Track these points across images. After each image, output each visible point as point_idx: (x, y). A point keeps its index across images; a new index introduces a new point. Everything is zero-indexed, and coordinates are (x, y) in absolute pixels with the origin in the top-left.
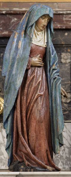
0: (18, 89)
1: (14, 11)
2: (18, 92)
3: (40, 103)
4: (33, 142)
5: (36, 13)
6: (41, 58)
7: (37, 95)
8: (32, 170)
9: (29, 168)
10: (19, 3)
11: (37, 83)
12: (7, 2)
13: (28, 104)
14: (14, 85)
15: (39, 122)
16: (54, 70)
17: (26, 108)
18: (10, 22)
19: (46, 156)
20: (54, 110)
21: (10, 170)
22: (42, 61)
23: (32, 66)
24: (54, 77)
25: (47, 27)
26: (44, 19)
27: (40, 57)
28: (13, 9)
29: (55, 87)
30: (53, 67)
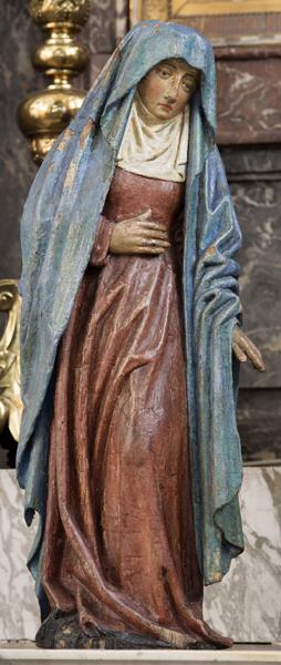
1: (242, 47)
4: (115, 539)
5: (133, 54)
7: (126, 360)
8: (102, 643)
9: (88, 636)
10: (266, 14)
11: (132, 316)
12: (225, 16)
13: (95, 396)
15: (134, 462)
16: (208, 265)
17: (88, 413)
19: (161, 589)
20: (204, 417)
21: (43, 640)
22: (164, 235)
23: (113, 254)
24: (207, 294)
26: (171, 75)
28: (239, 40)
29: (210, 332)
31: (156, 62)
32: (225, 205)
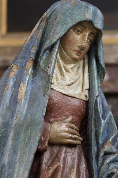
16: (107, 154)
23: (51, 144)
24: (109, 172)
25: (89, 53)
26: (82, 32)
27: (71, 122)
31: (74, 23)
32: (110, 118)
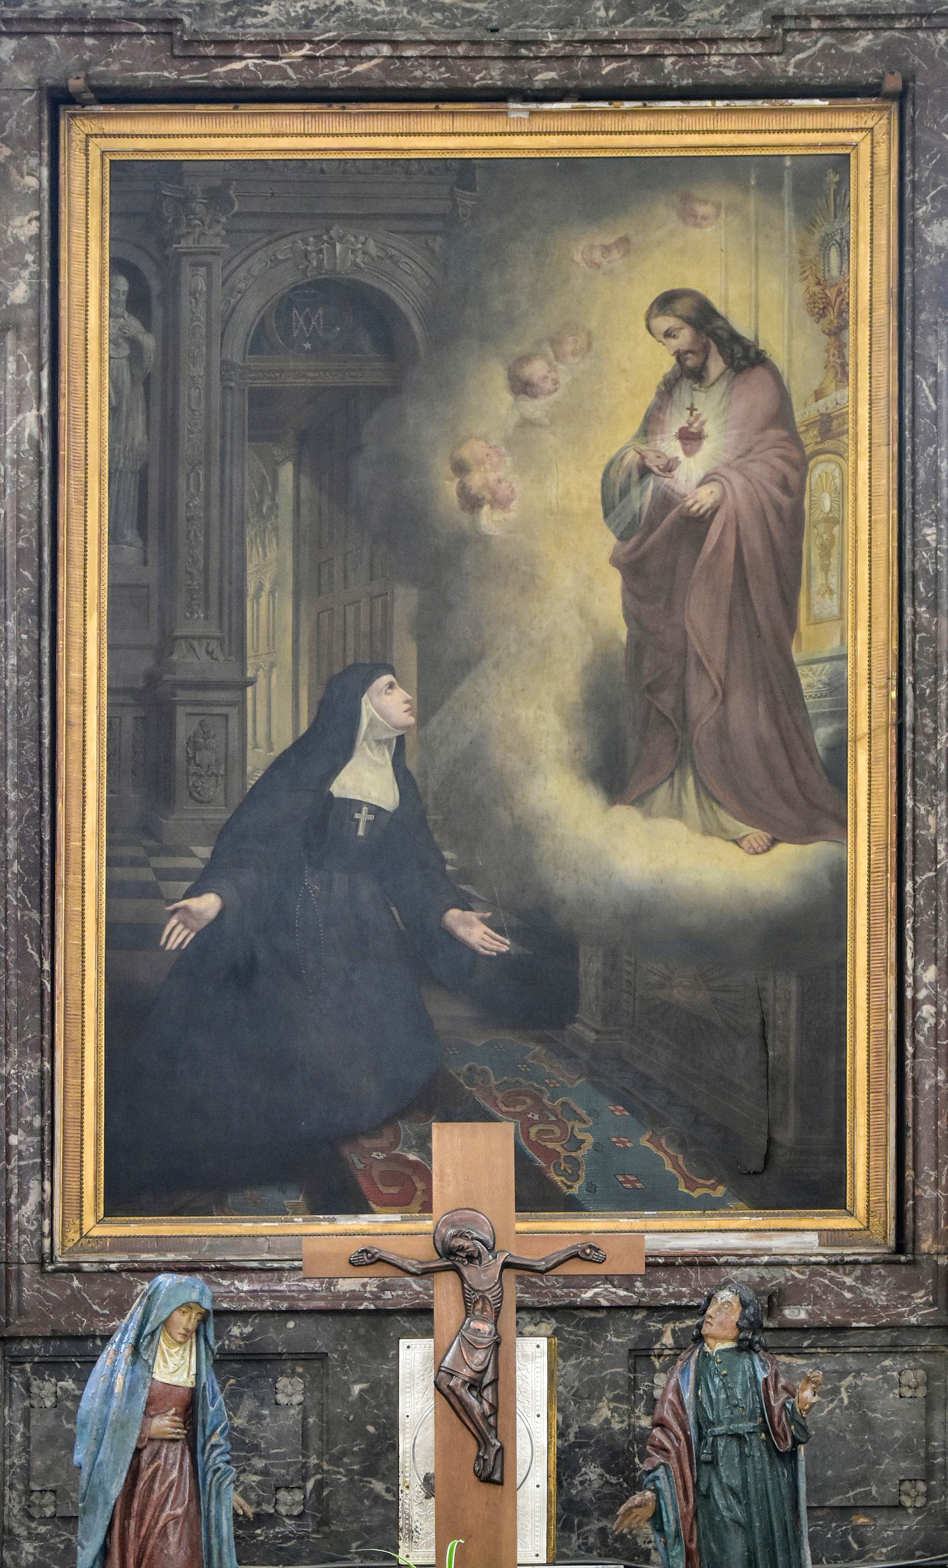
0: (113, 1502)
1: (142, 1262)
2: (115, 1506)
3: (173, 1539)
6: (177, 1418)
10: (157, 1237)
11: (167, 1484)
14: (106, 1492)
16: (214, 1447)
18: (130, 1292)
23: (151, 1440)
24: (215, 1467)
25: (197, 1332)
27: (174, 1415)
30: (214, 1440)
